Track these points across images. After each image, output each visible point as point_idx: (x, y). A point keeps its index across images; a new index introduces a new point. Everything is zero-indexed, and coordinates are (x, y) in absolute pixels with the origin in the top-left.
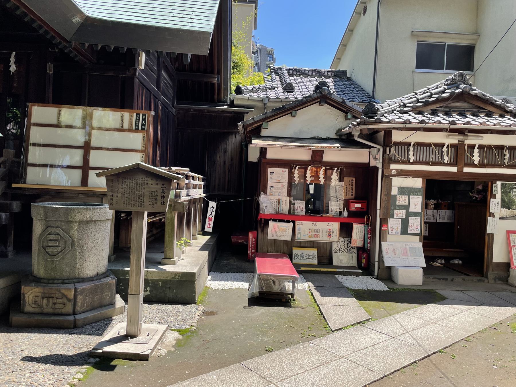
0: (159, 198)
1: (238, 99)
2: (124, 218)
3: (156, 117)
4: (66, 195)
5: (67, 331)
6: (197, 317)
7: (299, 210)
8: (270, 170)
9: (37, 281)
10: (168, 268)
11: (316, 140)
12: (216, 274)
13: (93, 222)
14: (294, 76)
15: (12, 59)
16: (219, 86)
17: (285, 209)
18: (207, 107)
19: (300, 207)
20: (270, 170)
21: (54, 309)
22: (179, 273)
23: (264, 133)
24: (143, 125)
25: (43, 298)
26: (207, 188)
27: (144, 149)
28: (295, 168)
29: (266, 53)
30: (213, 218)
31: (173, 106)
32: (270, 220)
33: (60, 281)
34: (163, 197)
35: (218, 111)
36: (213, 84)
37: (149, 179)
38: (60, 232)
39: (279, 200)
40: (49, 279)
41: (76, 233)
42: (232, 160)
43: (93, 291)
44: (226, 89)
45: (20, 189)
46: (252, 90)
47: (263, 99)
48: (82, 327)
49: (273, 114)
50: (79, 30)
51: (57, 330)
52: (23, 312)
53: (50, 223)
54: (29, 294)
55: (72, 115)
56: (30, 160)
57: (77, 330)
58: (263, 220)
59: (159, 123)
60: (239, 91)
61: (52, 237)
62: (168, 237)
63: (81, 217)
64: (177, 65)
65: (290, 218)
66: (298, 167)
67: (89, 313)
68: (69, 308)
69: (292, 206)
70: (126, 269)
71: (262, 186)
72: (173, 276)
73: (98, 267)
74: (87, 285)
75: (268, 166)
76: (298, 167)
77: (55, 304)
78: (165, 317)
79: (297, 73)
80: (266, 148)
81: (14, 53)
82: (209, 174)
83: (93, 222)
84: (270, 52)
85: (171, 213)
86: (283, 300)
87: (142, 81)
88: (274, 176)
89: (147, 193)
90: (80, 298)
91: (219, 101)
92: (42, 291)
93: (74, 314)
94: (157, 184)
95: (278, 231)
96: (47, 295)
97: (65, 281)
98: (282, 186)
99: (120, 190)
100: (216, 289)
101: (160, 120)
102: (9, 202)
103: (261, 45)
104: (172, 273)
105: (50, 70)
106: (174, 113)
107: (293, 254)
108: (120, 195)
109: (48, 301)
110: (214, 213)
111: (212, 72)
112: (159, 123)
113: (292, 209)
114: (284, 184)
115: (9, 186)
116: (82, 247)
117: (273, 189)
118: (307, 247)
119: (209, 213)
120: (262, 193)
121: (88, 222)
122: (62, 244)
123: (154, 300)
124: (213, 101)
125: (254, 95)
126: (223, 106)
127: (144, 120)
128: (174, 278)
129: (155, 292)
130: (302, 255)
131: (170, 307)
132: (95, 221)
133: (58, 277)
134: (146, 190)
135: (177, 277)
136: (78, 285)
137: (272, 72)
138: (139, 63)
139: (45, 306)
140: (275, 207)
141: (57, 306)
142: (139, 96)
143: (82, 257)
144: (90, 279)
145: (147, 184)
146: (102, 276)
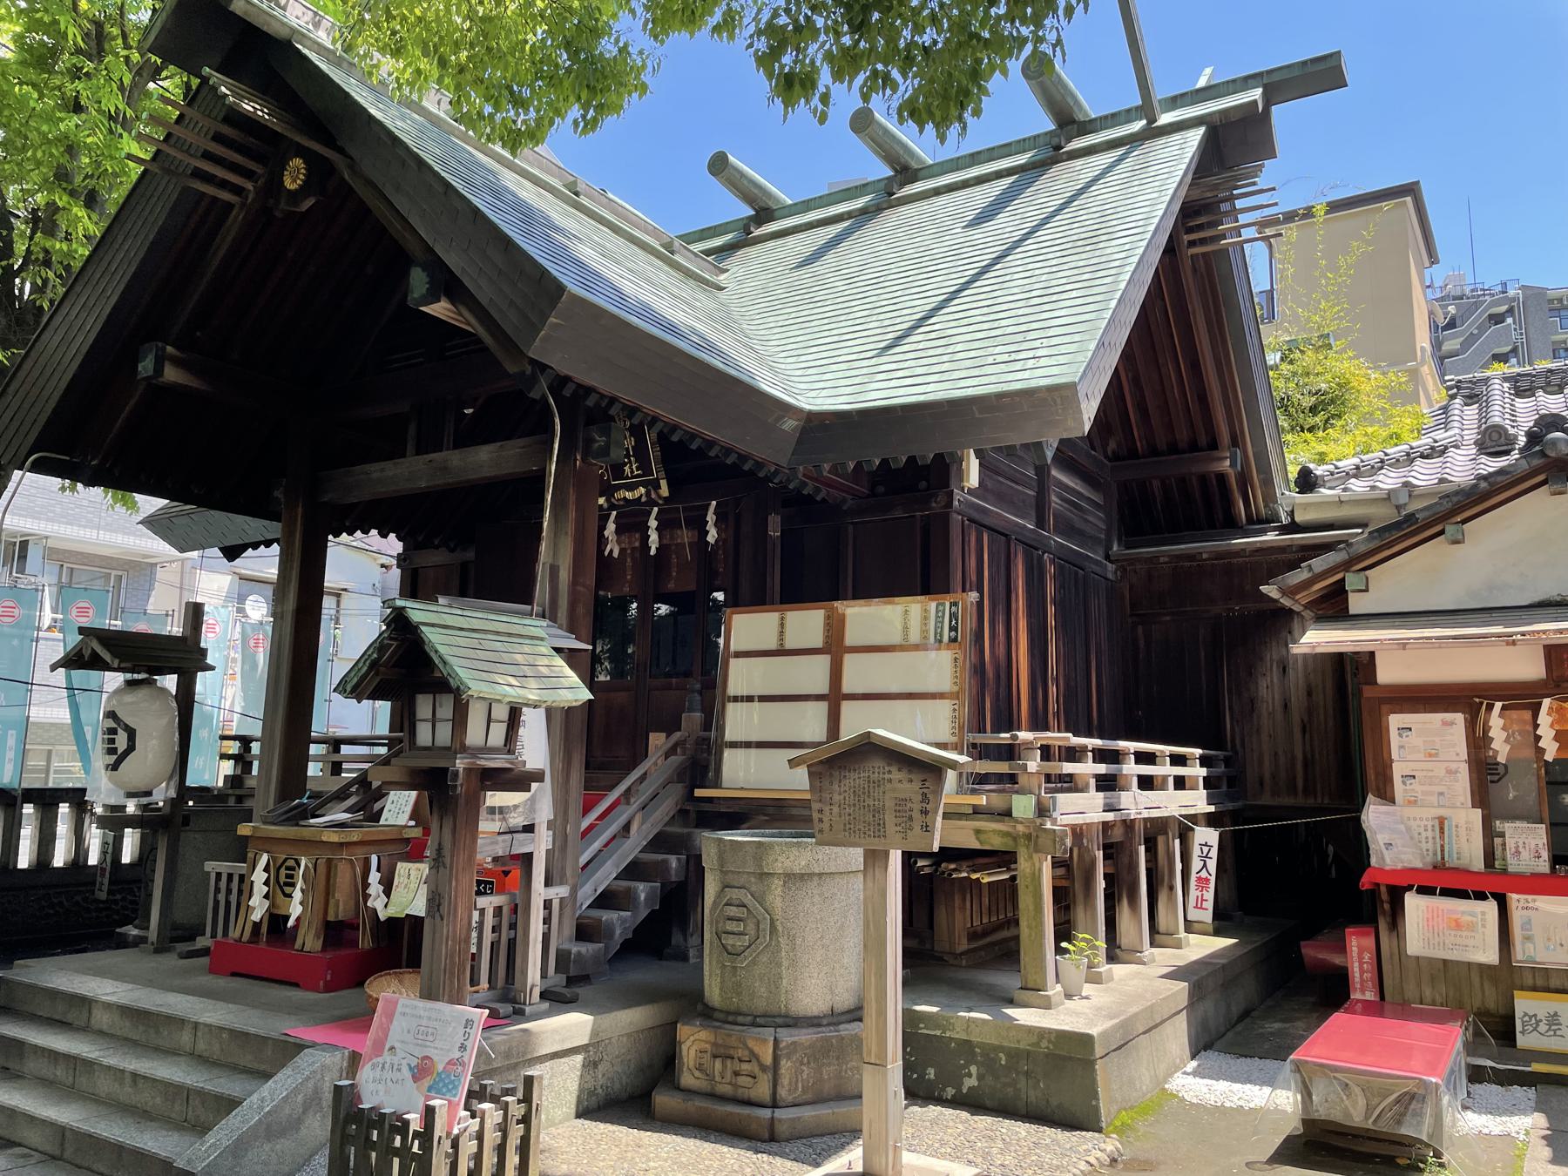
0: (916, 815)
1: (1306, 506)
2: (927, 870)
3: (980, 604)
4: (794, 811)
5: (753, 1143)
6: (1083, 1166)
7: (1525, 855)
8: (1395, 721)
9: (706, 1013)
10: (1024, 1016)
11: (1551, 610)
12: (1212, 1058)
13: (816, 878)
14: (1540, 393)
15: (711, 517)
16: (1244, 480)
17: (1468, 850)
18: (1205, 547)
19: (1528, 846)
20: (1395, 721)
21: (735, 1086)
22: (1050, 1031)
23: (1357, 604)
24: (951, 629)
25: (715, 1057)
26: (203, 792)
27: (956, 689)
28: (1490, 708)
29: (1546, 306)
30: (1213, 879)
31: (1107, 557)
32: (1410, 888)
33: (749, 1019)
34: (925, 812)
35: (1240, 552)
36: (1222, 478)
37: (894, 769)
38: (748, 900)
39: (1442, 821)
40: (728, 1013)
41: (778, 903)
42: (1309, 694)
43: (820, 1053)
44: (1268, 483)
45: (710, 800)
46: (1358, 472)
47: (1390, 492)
48: (788, 1140)
49: (1372, 546)
50: (799, 442)
51: (736, 1141)
52: (678, 1088)
53: (730, 878)
54: (688, 1043)
55: (807, 624)
56: (729, 736)
57: (775, 1146)
58: (1383, 889)
59: (1051, 610)
60: (1307, 482)
61: (733, 911)
62: (1029, 927)
63: (788, 863)
64: (1112, 445)
65: (1491, 884)
66: (1498, 705)
67: (809, 1107)
68: (762, 1090)
69: (1498, 841)
70: (918, 1008)
71: (1371, 775)
72: (1034, 1039)
73: (832, 992)
74: (805, 1036)
75: (1385, 708)
76: (1498, 705)
77: (736, 1074)
78: (995, 1151)
79: (1548, 384)
80: (1372, 654)
81: (714, 503)
82: (1238, 741)
83: (816, 878)
84: (1560, 300)
85: (1031, 857)
86: (1401, 1161)
87: (976, 516)
88: (1413, 739)
89: (890, 804)
90: (785, 1065)
91: (1250, 520)
92: (712, 1038)
93: (775, 1105)
94: (911, 781)
95: (1433, 928)
96: (722, 1051)
97: (758, 1020)
98: (1449, 772)
99: (836, 797)
100: (1195, 1101)
101: (1054, 602)
102: (686, 830)
103: (1523, 288)
104: (1030, 1030)
105: (774, 531)
106: (1110, 576)
107: (1518, 1014)
108: (836, 809)
109: (724, 1066)
110: (1212, 865)
111: (1214, 445)
112: (1051, 610)
113: (1498, 853)
114: (1454, 766)
115: (690, 796)
116: (792, 939)
117: (1414, 785)
118: (1548, 990)
119: (1196, 864)
120: (1370, 797)
121: (804, 877)
122: (751, 928)
123: (988, 1103)
124: (1232, 525)
125: (1358, 486)
126: (1264, 532)
127: (953, 616)
128: (1037, 1044)
129: (989, 1080)
130: (1554, 1019)
131: (1022, 1129)
132: (820, 875)
133: (745, 1009)
134: (887, 796)
135: (1044, 1044)
136: (782, 1032)
137: (1453, 397)
138: (961, 475)
139: (718, 1079)
140: (1430, 846)
141: (742, 1080)
142: (970, 554)
143: (793, 963)
144: (813, 1022)
145: (890, 781)
146: (844, 1018)
